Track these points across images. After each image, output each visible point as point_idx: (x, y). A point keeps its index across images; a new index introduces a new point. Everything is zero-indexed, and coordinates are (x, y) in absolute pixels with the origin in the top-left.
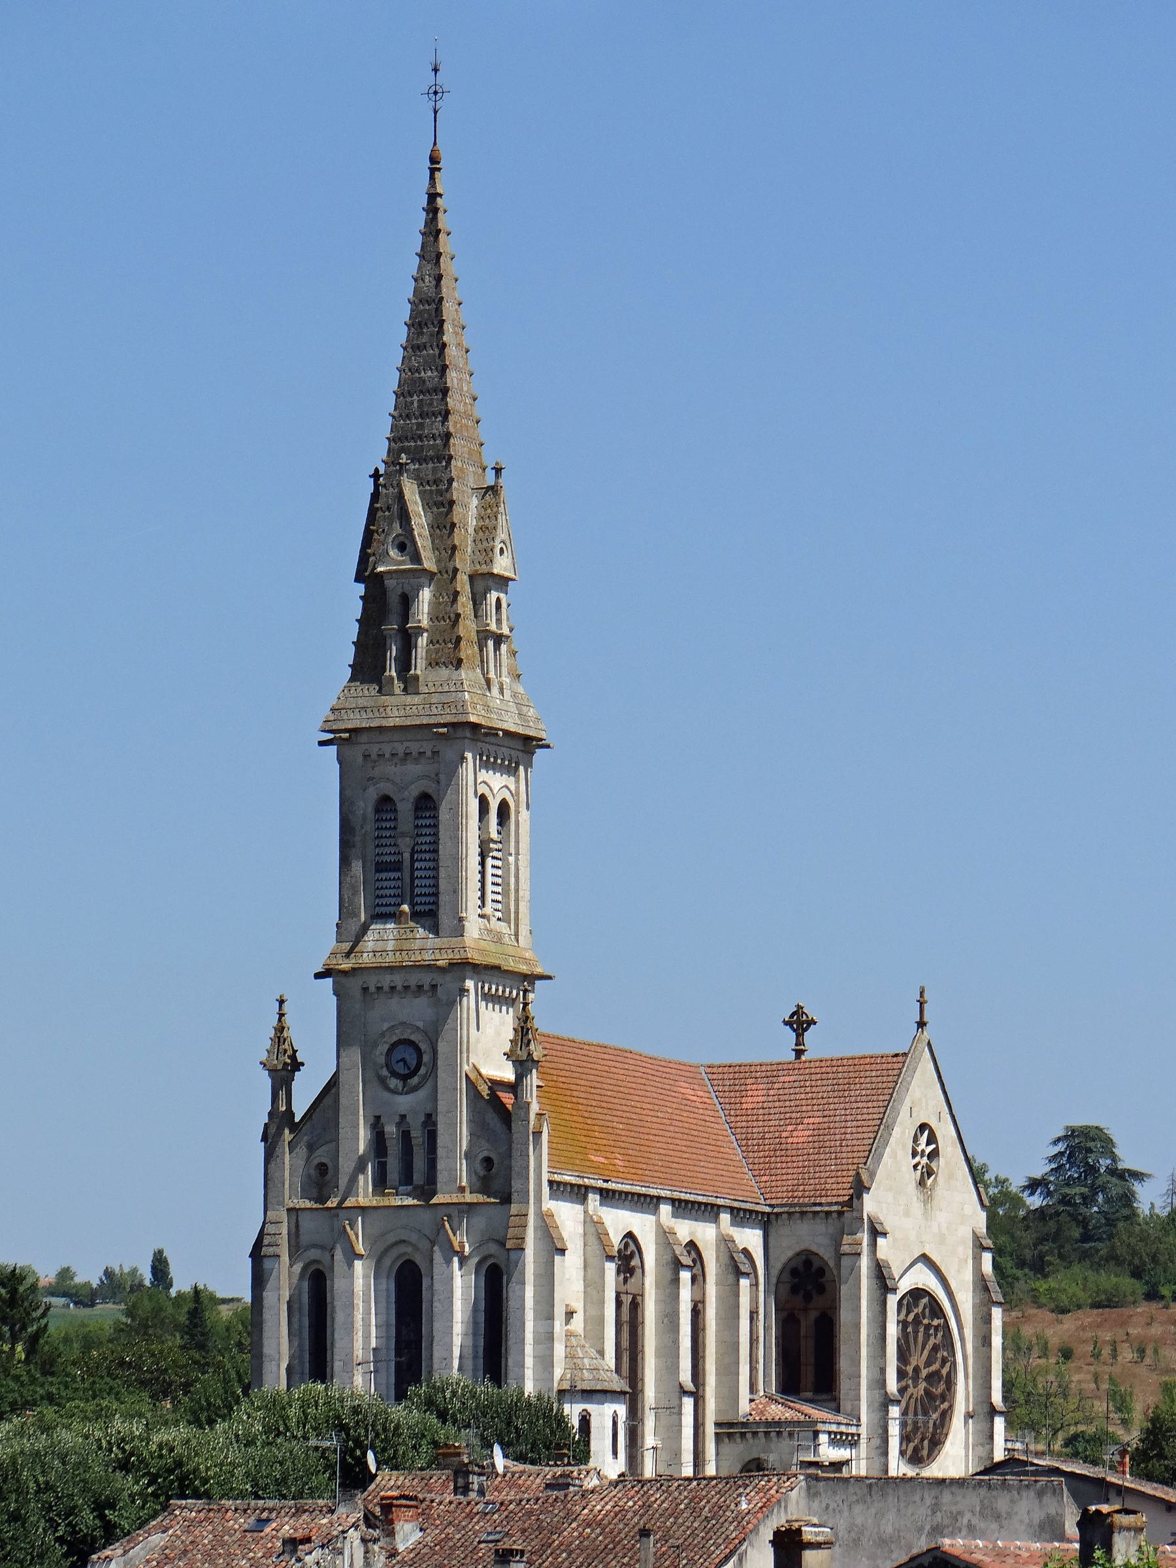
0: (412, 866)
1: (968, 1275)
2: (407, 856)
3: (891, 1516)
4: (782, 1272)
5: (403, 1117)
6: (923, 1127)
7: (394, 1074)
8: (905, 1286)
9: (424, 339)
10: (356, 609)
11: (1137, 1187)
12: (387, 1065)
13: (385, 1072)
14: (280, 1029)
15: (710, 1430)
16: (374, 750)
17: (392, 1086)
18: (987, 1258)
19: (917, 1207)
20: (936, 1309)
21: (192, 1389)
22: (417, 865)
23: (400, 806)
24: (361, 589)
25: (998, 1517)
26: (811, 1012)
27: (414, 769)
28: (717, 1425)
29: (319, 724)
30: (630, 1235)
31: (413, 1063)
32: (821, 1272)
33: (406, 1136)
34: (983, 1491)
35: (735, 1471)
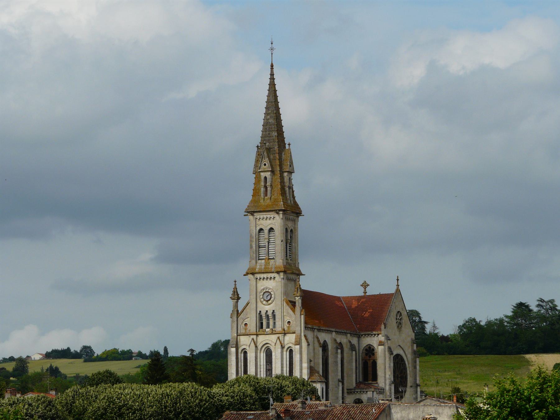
1: (410, 350)
3: (412, 414)
4: (363, 349)
5: (267, 311)
6: (398, 312)
7: (264, 300)
8: (395, 353)
10: (253, 181)
11: (426, 325)
13: (262, 300)
14: (235, 288)
15: (345, 391)
16: (258, 217)
18: (415, 345)
19: (397, 333)
20: (402, 360)
21: (526, 393)
23: (265, 231)
24: (254, 176)
25: (439, 414)
26: (368, 282)
27: (268, 222)
28: (347, 390)
29: (244, 210)
30: (325, 341)
32: (373, 350)
33: (267, 316)
34: (435, 407)
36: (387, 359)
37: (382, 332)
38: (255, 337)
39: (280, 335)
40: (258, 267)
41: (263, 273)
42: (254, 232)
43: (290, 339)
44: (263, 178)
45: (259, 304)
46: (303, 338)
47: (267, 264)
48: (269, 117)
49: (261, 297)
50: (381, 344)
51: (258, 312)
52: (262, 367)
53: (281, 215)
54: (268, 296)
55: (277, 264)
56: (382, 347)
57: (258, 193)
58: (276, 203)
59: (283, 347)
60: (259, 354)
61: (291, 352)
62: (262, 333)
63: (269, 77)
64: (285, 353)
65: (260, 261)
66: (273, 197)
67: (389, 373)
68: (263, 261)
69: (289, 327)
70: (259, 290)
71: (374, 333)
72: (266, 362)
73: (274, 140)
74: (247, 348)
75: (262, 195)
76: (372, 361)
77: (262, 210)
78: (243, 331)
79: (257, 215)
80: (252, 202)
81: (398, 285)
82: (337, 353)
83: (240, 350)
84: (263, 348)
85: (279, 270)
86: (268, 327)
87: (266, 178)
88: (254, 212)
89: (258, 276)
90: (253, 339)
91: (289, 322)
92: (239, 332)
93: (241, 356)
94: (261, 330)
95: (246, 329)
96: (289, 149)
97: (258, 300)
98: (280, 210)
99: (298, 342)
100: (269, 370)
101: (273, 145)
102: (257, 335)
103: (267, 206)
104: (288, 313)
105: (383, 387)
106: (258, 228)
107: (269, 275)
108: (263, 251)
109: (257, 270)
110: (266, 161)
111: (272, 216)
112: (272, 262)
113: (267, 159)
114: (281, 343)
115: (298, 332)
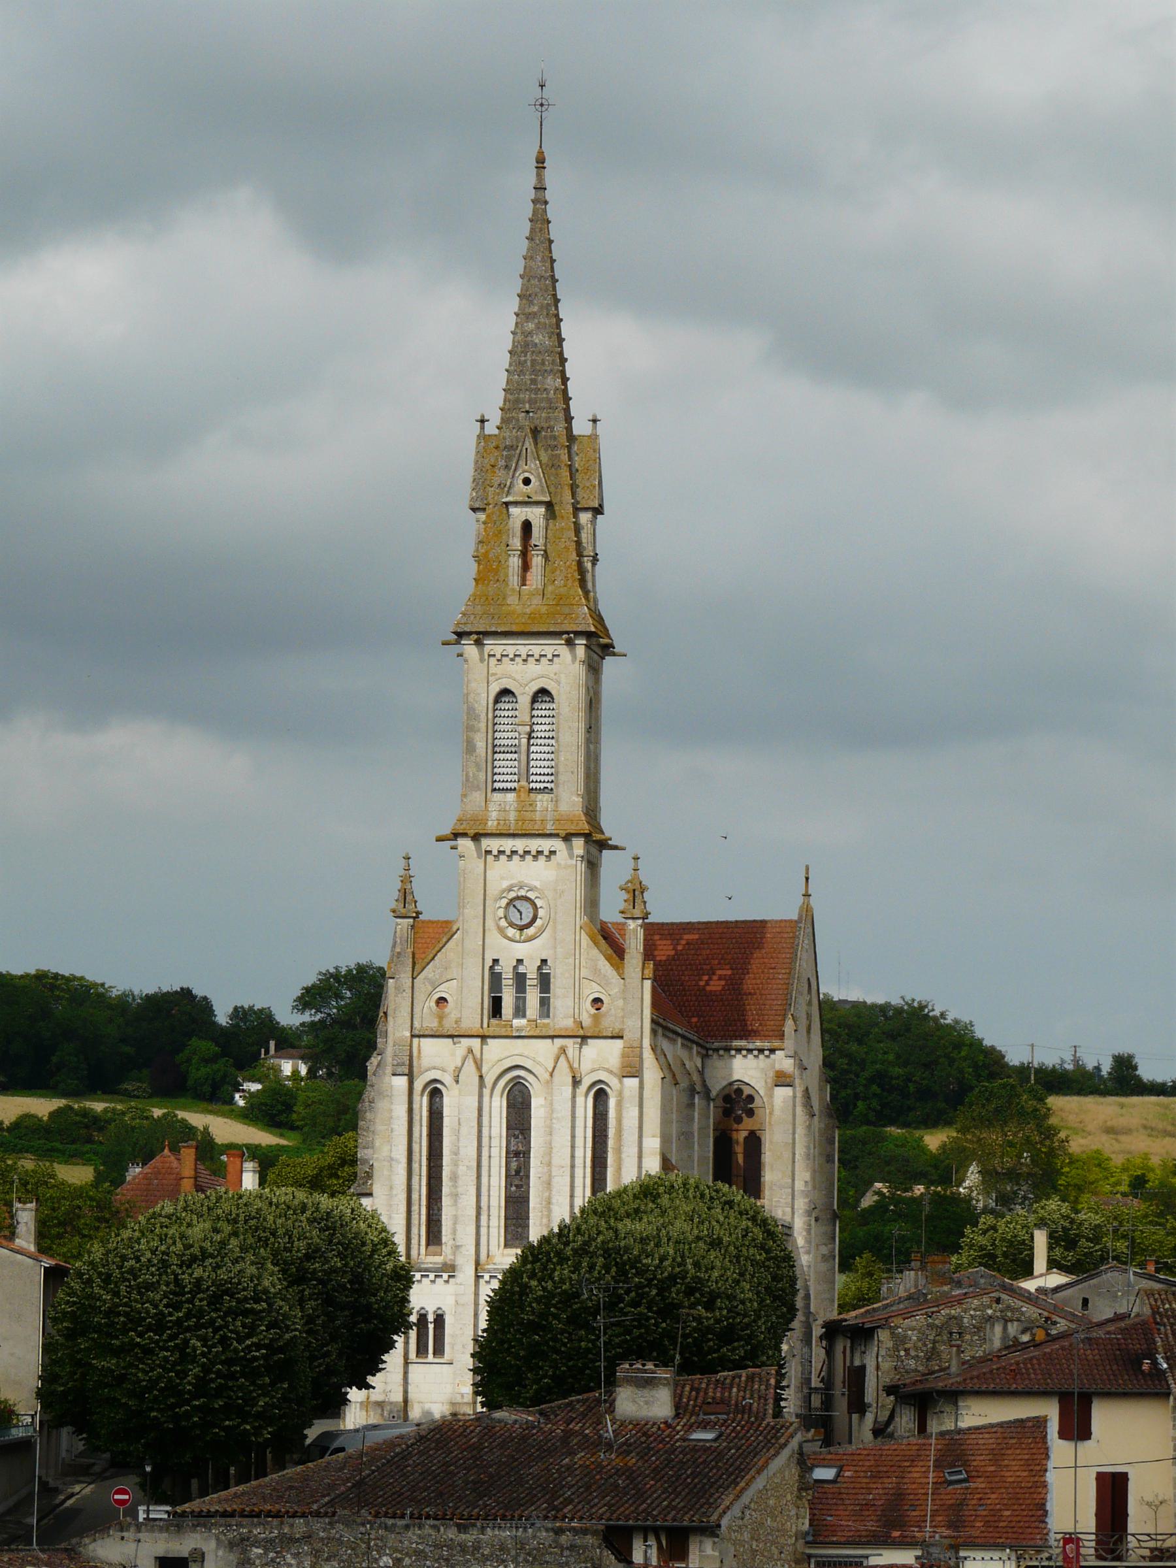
0: (528, 750)
2: (524, 741)
5: (520, 961)
7: (512, 925)
9: (535, 309)
12: (505, 917)
13: (503, 923)
14: (407, 879)
17: (510, 935)
22: (533, 748)
27: (532, 668)
31: (526, 921)
33: (520, 980)
35: (603, 923)
36: (800, 1131)
37: (789, 1043)
38: (477, 1042)
39: (569, 1042)
40: (494, 815)
41: (514, 835)
42: (483, 697)
43: (600, 1058)
44: (517, 526)
45: (494, 937)
46: (648, 1054)
47: (524, 808)
48: (531, 326)
49: (501, 913)
50: (782, 1080)
51: (489, 963)
52: (495, 1142)
53: (581, 651)
54: (522, 913)
55: (564, 807)
56: (786, 1092)
57: (496, 572)
58: (566, 610)
59: (576, 1083)
60: (486, 1099)
61: (601, 1096)
62: (503, 1032)
63: (532, 194)
64: (580, 1100)
65: (497, 796)
66: (550, 588)
67: (807, 1176)
68: (511, 796)
69: (596, 1019)
70: (492, 891)
71: (758, 1044)
72: (508, 1129)
73: (549, 401)
74: (447, 1079)
75: (514, 580)
76: (744, 1134)
77: (514, 628)
78: (432, 1024)
79: (494, 646)
80: (474, 598)
81: (807, 895)
82: (691, 1105)
83: (418, 1085)
84: (502, 1083)
85: (573, 828)
86: (520, 1011)
87: (527, 526)
88: (487, 634)
89: (494, 844)
90: (470, 1051)
91: (597, 1001)
92: (417, 1024)
93: (422, 1104)
94: (494, 1021)
95: (441, 1018)
96: (594, 437)
97: (490, 923)
98: (578, 634)
99: (632, 1069)
100: (517, 1154)
101: (548, 419)
102: (484, 1038)
103: (533, 617)
104: (596, 970)
105: (788, 1218)
106: (495, 688)
107: (534, 844)
108: (507, 765)
109: (491, 825)
110: (531, 468)
111: (549, 651)
112: (542, 801)
113: (533, 465)
114: (571, 1067)
115: (631, 1035)
